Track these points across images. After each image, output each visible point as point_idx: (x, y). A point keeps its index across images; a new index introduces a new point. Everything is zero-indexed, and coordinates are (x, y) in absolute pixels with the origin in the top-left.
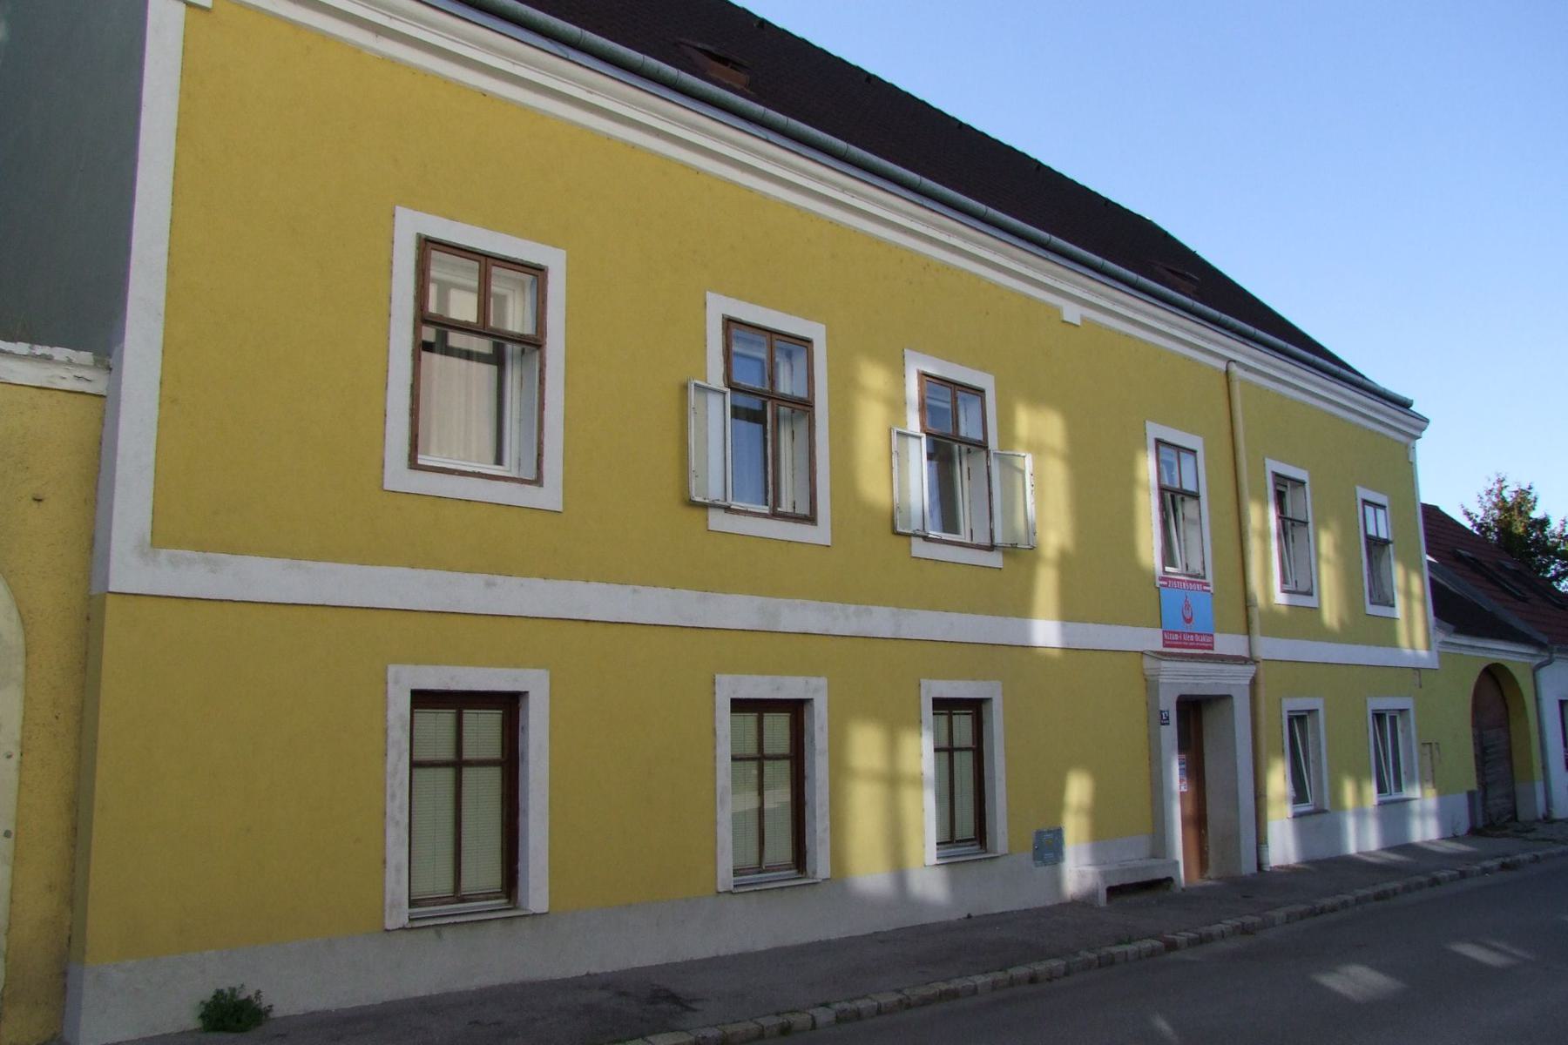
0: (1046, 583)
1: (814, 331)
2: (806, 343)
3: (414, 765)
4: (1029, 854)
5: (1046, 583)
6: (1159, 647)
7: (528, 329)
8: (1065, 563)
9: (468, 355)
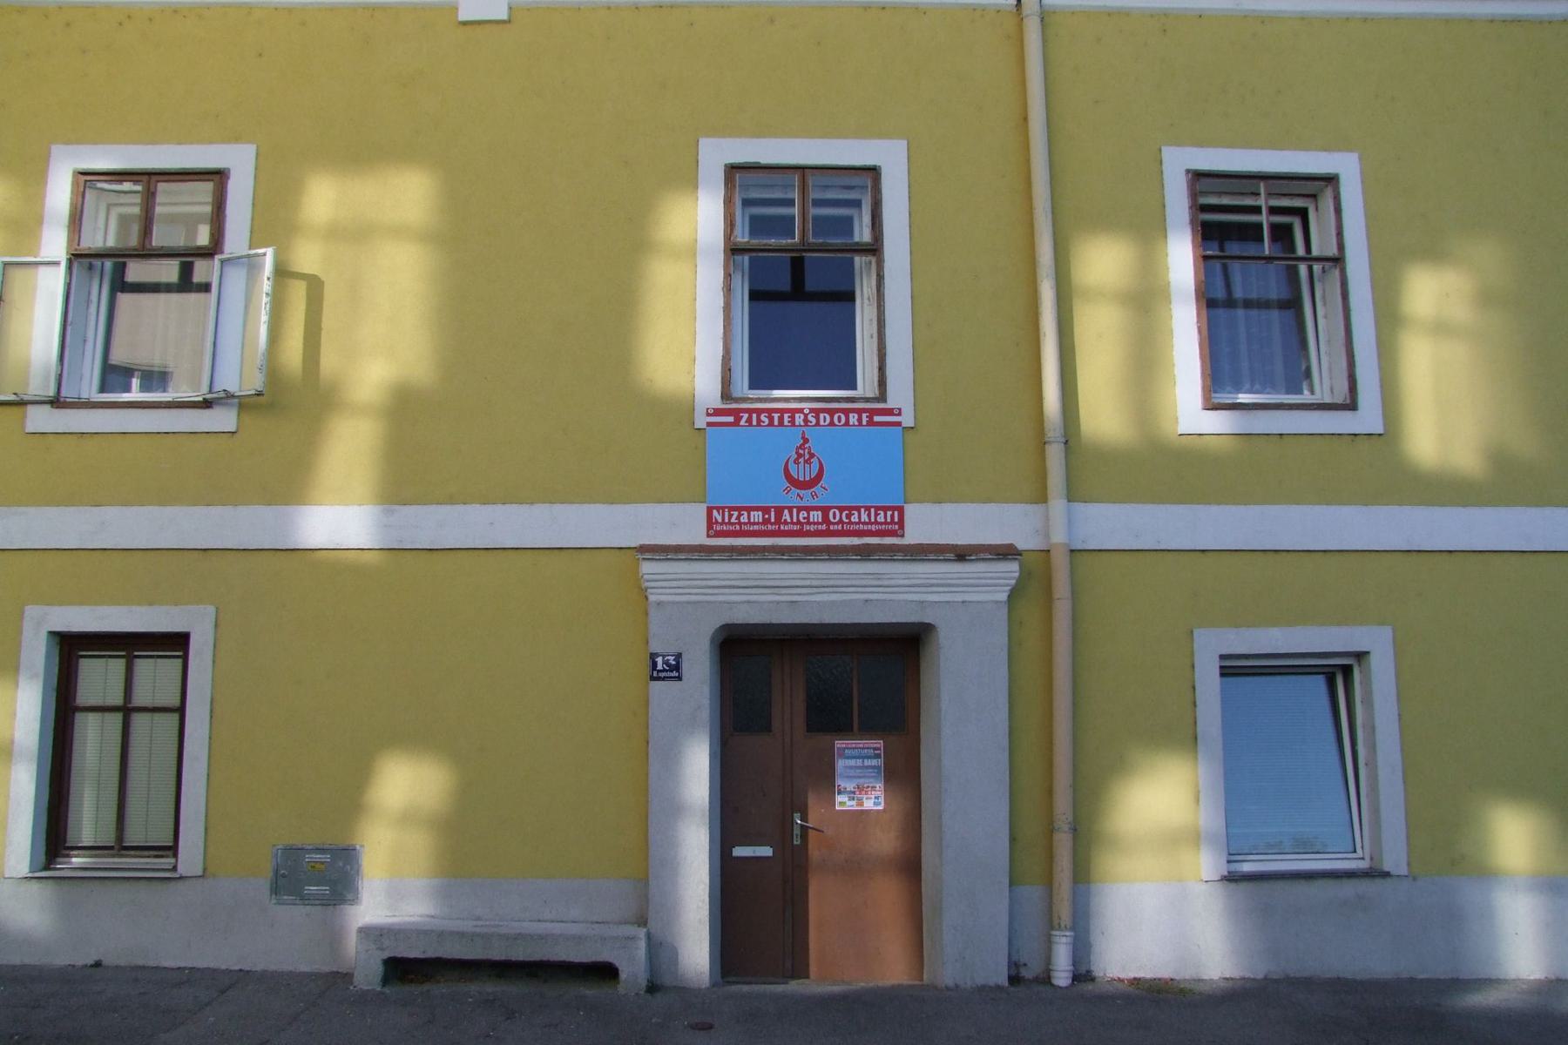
0: (351, 447)
1: (1345, 165)
2: (1331, 180)
3: (181, 710)
4: (263, 883)
5: (351, 447)
6: (696, 533)
7: (1332, 251)
8: (405, 410)
9: (155, 288)
